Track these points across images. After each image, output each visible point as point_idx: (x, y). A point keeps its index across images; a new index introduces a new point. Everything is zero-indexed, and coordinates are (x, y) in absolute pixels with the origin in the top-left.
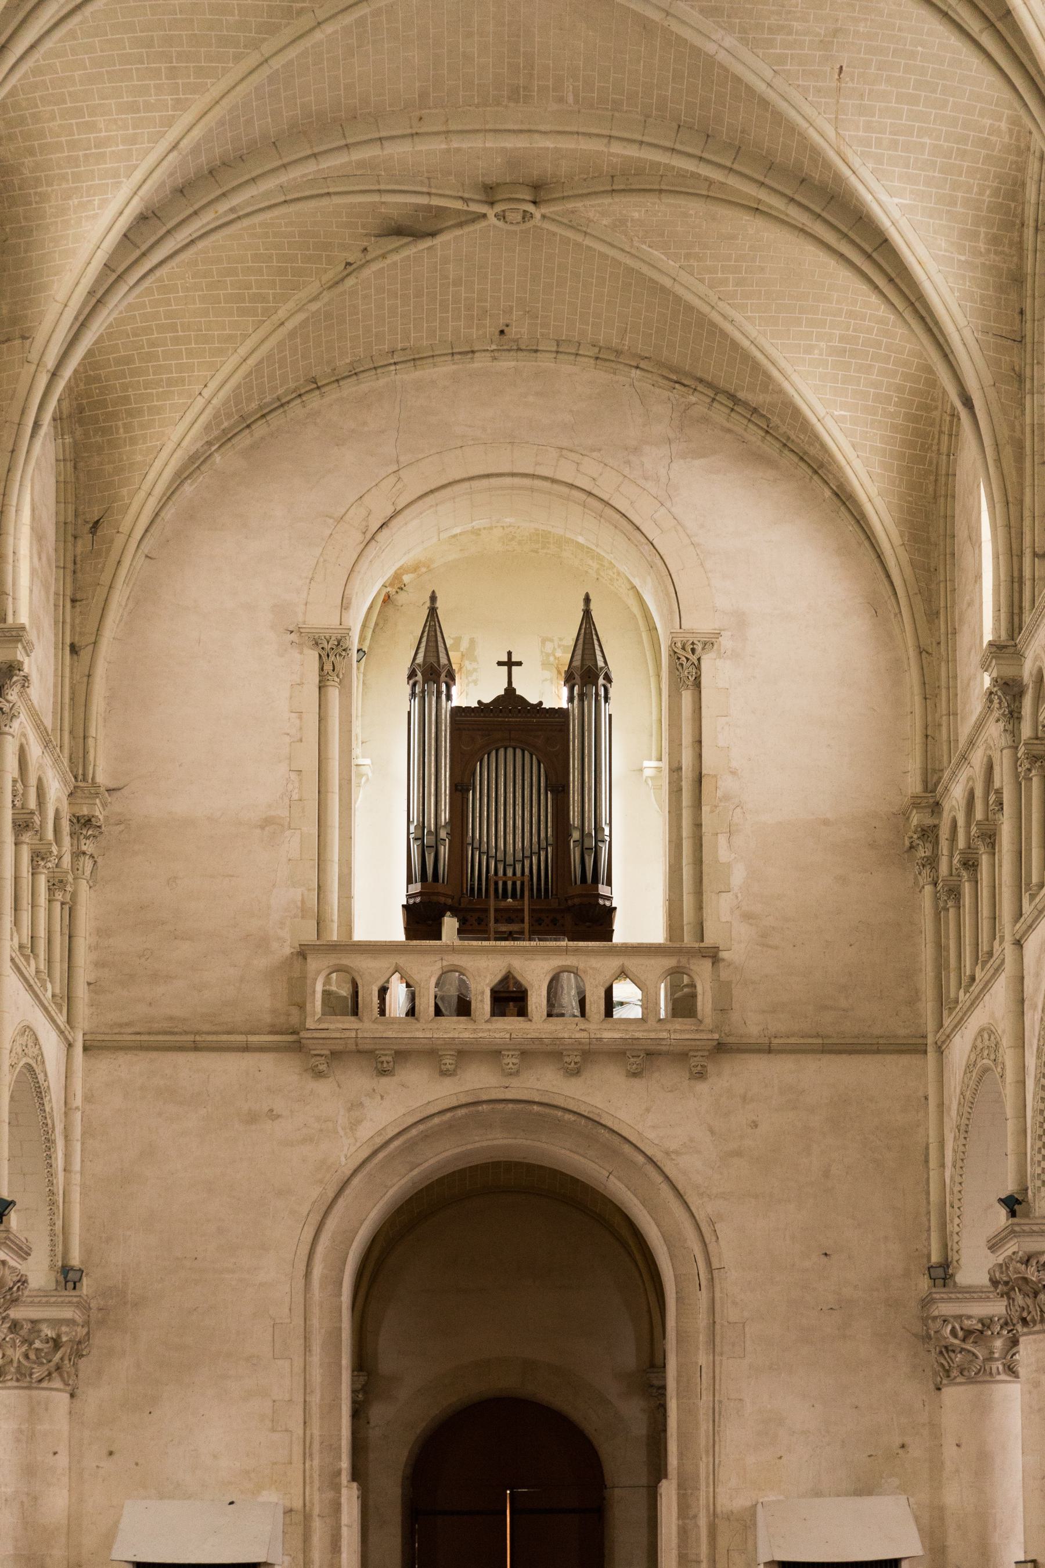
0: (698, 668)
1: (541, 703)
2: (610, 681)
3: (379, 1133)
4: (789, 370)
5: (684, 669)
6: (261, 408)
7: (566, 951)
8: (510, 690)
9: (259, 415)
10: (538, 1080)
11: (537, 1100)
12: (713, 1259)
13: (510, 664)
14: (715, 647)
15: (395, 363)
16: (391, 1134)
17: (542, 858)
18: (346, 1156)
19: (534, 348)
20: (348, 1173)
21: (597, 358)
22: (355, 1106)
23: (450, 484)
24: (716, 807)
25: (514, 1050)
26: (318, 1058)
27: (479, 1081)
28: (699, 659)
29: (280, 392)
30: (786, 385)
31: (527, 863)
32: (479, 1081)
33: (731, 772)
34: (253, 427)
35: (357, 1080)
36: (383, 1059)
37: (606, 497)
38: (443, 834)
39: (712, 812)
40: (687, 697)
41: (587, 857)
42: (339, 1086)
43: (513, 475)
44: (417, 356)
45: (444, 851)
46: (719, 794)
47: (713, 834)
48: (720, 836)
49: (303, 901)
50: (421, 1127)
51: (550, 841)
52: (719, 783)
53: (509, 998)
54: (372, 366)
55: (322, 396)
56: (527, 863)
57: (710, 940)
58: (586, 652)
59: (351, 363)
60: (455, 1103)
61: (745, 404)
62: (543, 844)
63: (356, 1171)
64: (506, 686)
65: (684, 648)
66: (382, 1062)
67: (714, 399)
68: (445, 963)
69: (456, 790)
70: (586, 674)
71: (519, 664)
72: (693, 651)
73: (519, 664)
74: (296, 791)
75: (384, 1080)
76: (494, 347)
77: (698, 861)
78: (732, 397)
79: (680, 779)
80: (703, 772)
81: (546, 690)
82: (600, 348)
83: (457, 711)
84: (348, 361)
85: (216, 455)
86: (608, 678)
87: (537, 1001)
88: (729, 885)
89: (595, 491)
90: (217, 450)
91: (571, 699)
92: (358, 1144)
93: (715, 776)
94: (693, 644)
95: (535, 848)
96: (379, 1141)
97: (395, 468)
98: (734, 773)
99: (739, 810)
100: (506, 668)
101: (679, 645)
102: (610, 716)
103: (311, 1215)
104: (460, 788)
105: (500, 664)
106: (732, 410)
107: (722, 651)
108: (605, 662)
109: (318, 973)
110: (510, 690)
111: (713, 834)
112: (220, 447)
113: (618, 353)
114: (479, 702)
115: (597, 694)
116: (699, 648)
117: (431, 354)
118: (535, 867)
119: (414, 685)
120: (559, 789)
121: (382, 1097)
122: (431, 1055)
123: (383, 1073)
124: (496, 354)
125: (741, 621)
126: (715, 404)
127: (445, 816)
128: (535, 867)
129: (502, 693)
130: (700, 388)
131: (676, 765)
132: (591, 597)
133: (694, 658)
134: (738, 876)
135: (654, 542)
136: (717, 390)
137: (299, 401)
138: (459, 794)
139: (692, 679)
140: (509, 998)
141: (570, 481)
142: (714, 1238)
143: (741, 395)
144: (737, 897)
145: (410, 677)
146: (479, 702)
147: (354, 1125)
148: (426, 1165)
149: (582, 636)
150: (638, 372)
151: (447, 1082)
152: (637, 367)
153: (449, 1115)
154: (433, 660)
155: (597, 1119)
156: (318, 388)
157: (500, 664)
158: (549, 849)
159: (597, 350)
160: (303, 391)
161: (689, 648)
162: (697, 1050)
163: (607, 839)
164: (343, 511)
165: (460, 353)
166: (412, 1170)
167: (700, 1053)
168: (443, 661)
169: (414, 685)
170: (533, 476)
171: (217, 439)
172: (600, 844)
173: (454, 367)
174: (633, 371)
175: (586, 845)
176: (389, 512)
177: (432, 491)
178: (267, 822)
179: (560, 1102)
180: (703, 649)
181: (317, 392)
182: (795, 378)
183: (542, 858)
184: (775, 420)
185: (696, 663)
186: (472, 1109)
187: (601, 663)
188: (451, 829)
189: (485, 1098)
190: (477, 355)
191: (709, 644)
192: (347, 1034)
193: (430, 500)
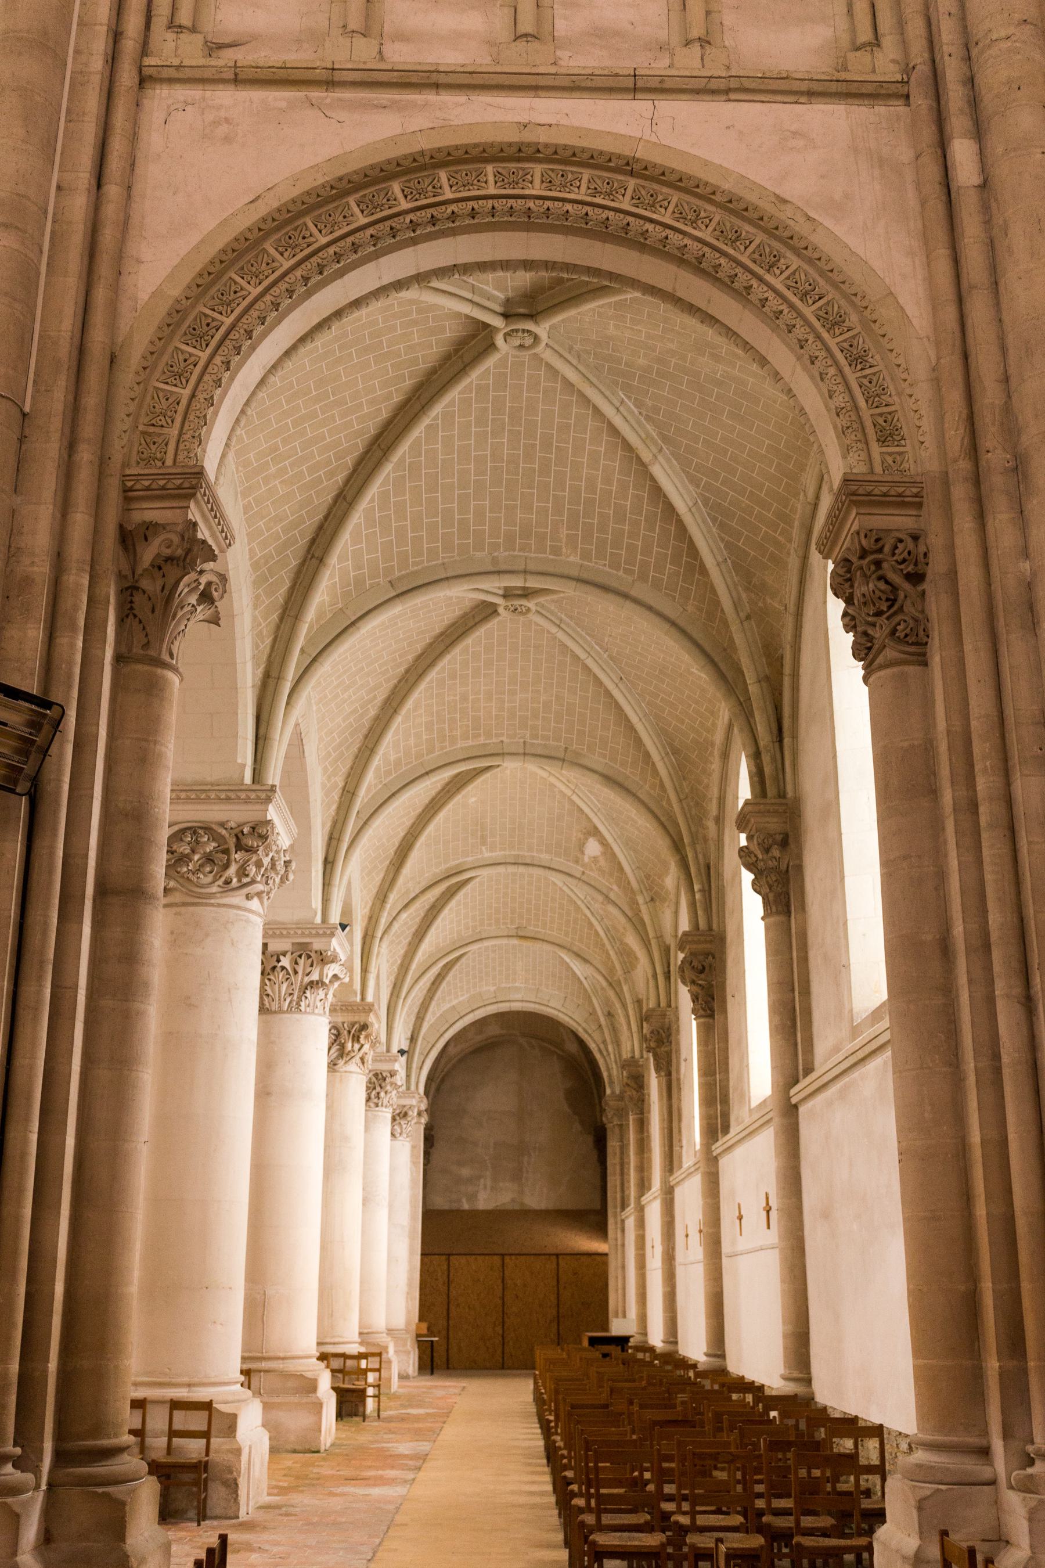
40: (644, 436)
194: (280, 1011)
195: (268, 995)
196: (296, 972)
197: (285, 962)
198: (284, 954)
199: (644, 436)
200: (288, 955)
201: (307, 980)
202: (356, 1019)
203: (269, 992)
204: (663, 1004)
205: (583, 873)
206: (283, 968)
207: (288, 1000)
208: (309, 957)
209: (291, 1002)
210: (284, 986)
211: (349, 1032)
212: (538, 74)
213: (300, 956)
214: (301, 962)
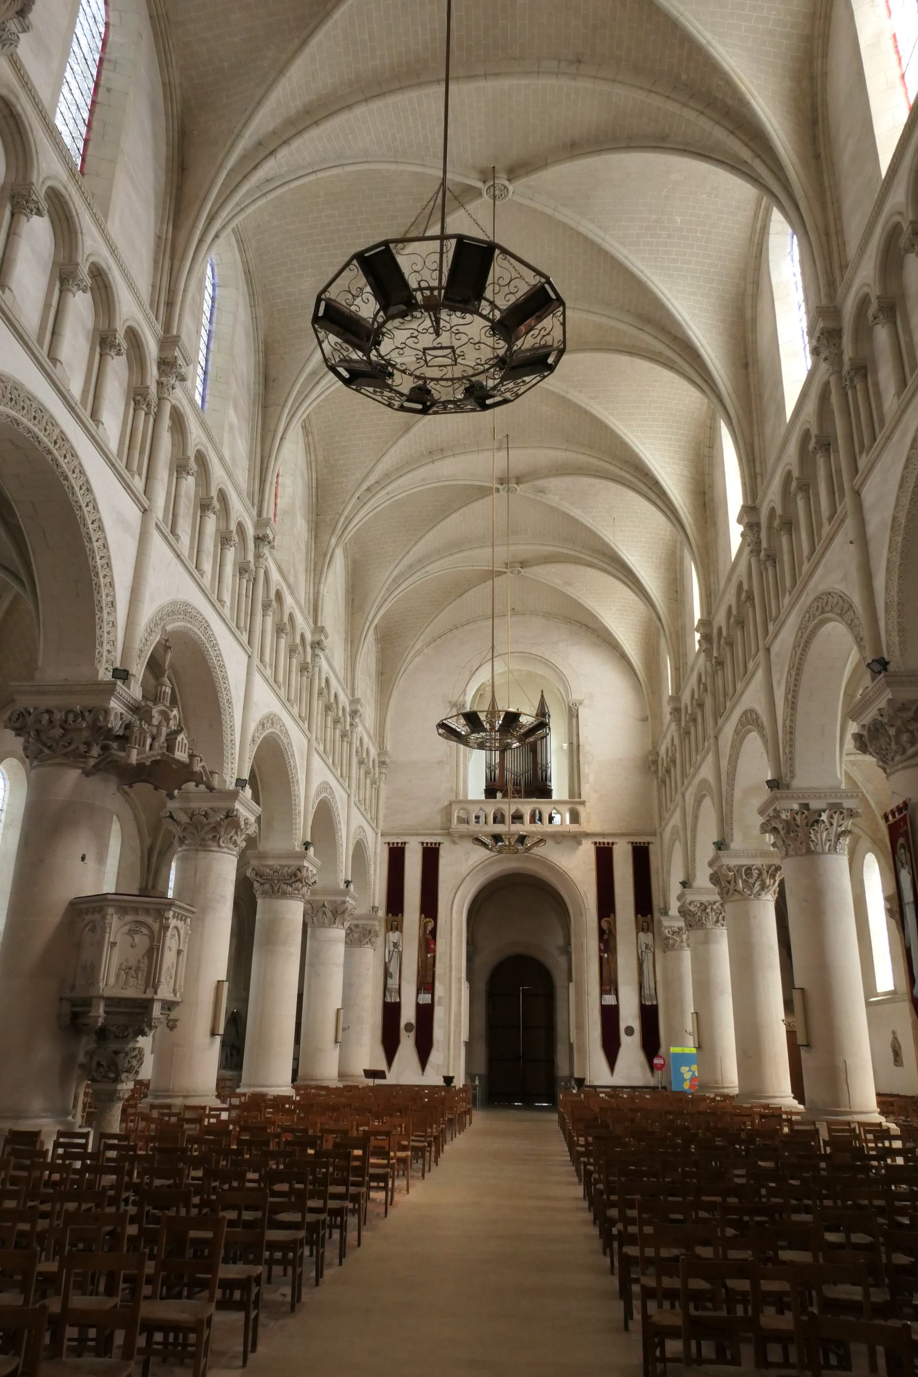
5: (573, 714)
40: (574, 720)
57: (583, 799)
87: (527, 818)
96: (475, 865)
134: (592, 778)
178: (440, 762)
194: (823, 852)
195: (812, 841)
196: (832, 824)
197: (824, 817)
198: (824, 811)
199: (574, 720)
200: (827, 812)
201: (840, 829)
202: (771, 863)
203: (814, 838)
204: (150, 886)
205: (113, 944)
206: (823, 821)
207: (828, 845)
208: (842, 813)
209: (830, 846)
210: (825, 834)
211: (768, 872)
212: (417, 835)
213: (835, 813)
214: (836, 817)
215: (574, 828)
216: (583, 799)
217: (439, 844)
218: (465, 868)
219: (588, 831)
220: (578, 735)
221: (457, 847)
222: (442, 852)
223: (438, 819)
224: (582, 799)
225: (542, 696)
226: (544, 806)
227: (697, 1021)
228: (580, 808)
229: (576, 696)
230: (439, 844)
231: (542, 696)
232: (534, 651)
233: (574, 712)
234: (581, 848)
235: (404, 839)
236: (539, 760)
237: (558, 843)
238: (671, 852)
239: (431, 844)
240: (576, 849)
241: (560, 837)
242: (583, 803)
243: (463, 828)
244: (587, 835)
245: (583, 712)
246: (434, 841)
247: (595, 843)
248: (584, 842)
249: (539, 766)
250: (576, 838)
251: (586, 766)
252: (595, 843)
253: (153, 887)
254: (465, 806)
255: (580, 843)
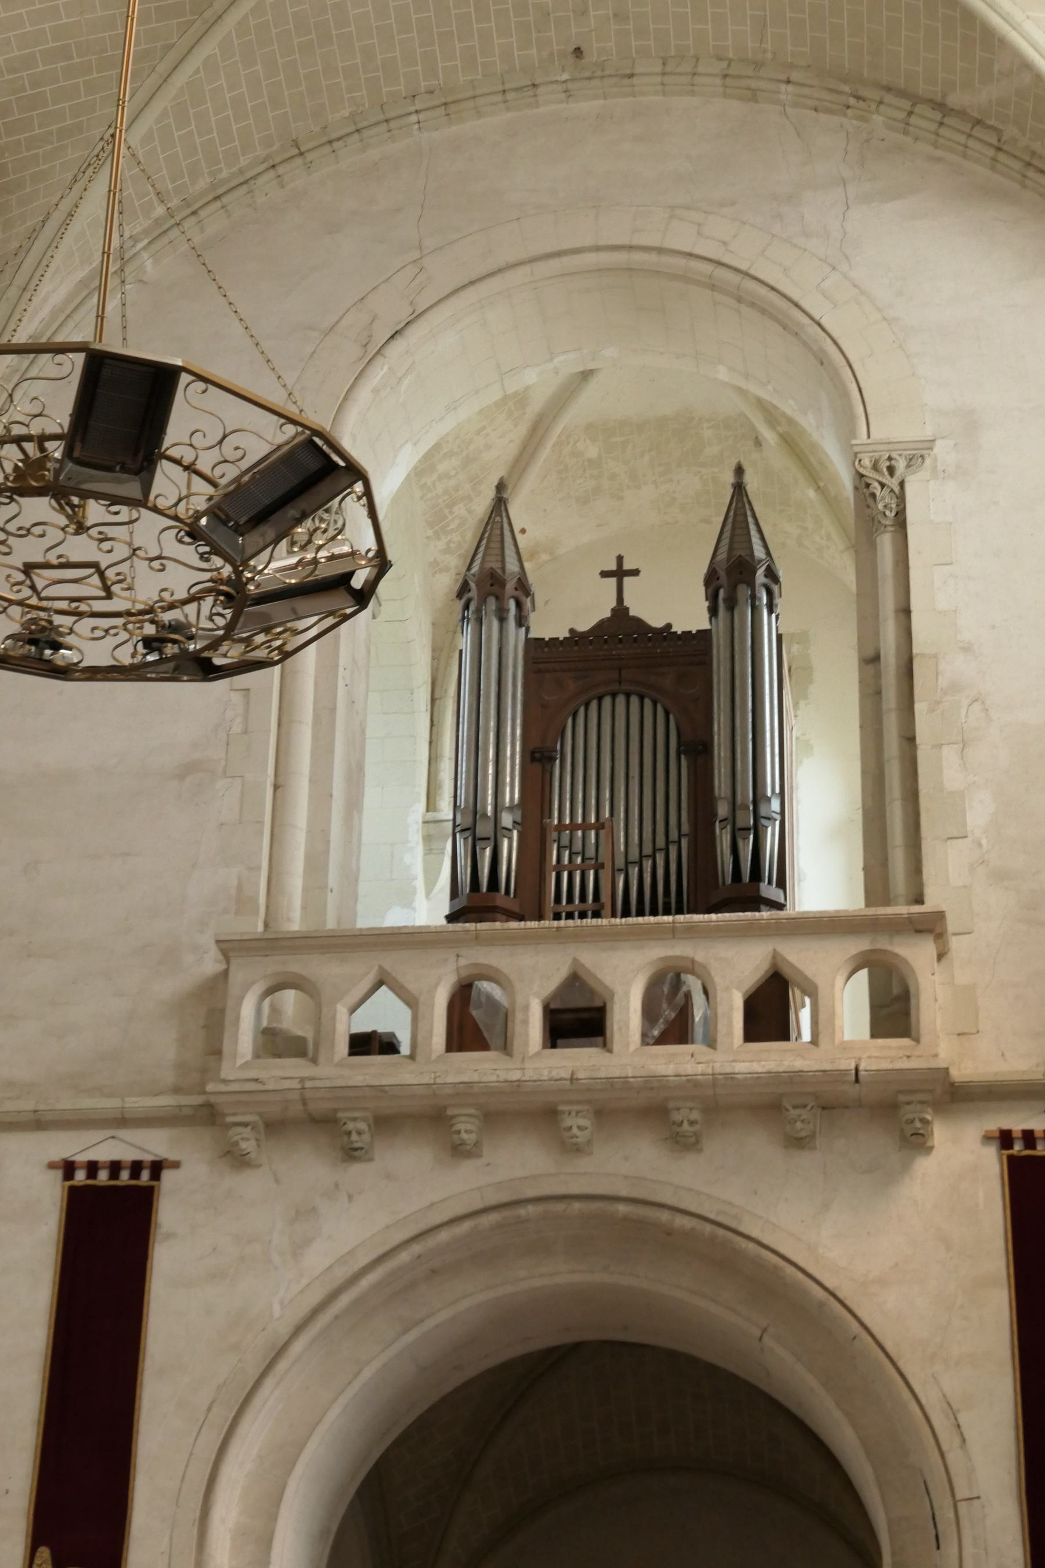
0: (901, 498)
1: (669, 626)
2: (776, 579)
3: (342, 1260)
4: (1019, 16)
5: (878, 513)
6: (213, 186)
7: (673, 932)
8: (620, 611)
9: (210, 197)
10: (626, 1158)
11: (624, 1193)
12: (958, 1482)
13: (620, 573)
14: (928, 461)
15: (417, 112)
16: (363, 1260)
17: (673, 856)
18: (281, 1303)
19: (628, 71)
20: (284, 1330)
21: (725, 76)
22: (304, 1213)
23: (500, 271)
24: (938, 703)
25: (579, 1102)
26: (240, 1129)
27: (519, 1164)
28: (902, 484)
29: (243, 161)
30: (1014, 37)
31: (648, 865)
32: (519, 1164)
33: (962, 648)
34: (203, 213)
35: (307, 1168)
36: (350, 1126)
37: (743, 267)
38: (507, 819)
39: (932, 710)
40: (886, 542)
41: (740, 843)
42: (277, 1181)
43: (597, 249)
44: (449, 99)
45: (509, 848)
46: (943, 682)
47: (934, 747)
48: (945, 750)
49: (240, 888)
50: (417, 1248)
51: (685, 828)
52: (942, 666)
53: (577, 1020)
54: (382, 117)
55: (308, 166)
56: (648, 865)
57: (933, 901)
58: (738, 532)
59: (352, 115)
60: (478, 1205)
61: (961, 113)
62: (674, 835)
63: (298, 1330)
64: (613, 603)
65: (875, 467)
66: (349, 1133)
67: (910, 113)
68: (463, 962)
69: (533, 759)
70: (737, 576)
71: (635, 573)
72: (891, 470)
73: (635, 573)
74: (239, 719)
75: (356, 1169)
76: (565, 76)
77: (912, 796)
78: (940, 106)
79: (878, 675)
80: (915, 651)
81: (673, 601)
82: (730, 61)
83: (535, 647)
84: (346, 113)
85: (145, 255)
86: (771, 574)
87: (627, 1016)
88: (965, 825)
89: (727, 259)
90: (144, 248)
91: (713, 611)
92: (304, 1282)
93: (935, 657)
94: (890, 459)
95: (661, 842)
96: (342, 1274)
97: (416, 255)
98: (967, 649)
99: (977, 706)
100: (613, 581)
101: (867, 462)
102: (779, 637)
103: (214, 1410)
104: (539, 758)
105: (605, 574)
106: (941, 124)
107: (940, 468)
108: (768, 553)
109: (247, 987)
110: (620, 611)
111: (934, 747)
112: (150, 243)
113: (758, 65)
114: (572, 631)
115: (754, 597)
116: (901, 465)
117: (470, 94)
118: (660, 872)
119: (467, 607)
120: (697, 749)
121: (350, 1198)
122: (429, 1119)
123: (351, 1154)
124: (570, 85)
125: (970, 424)
126: (913, 120)
127: (512, 793)
128: (660, 872)
129: (608, 614)
130: (889, 98)
131: (870, 653)
132: (744, 467)
133: (893, 483)
134: (979, 814)
135: (823, 322)
136: (916, 100)
137: (272, 174)
138: (537, 767)
139: (891, 515)
140: (577, 1020)
141: (687, 249)
142: (957, 1441)
143: (954, 100)
144: (980, 845)
145: (460, 595)
146: (572, 631)
147: (298, 1248)
148: (430, 1324)
149: (730, 520)
150: (790, 88)
151: (467, 1167)
152: (788, 82)
153: (467, 1225)
154: (496, 566)
155: (733, 1224)
156: (301, 154)
157: (605, 574)
158: (684, 842)
159: (725, 64)
160: (278, 160)
161: (884, 465)
162: (913, 1092)
163: (778, 817)
164: (335, 318)
165: (517, 90)
166: (406, 1331)
167: (919, 1097)
168: (512, 566)
169: (467, 607)
170: (630, 248)
171: (146, 232)
172: (764, 822)
173: (510, 115)
174: (783, 87)
175: (740, 824)
176: (404, 315)
177: (472, 283)
178: (187, 769)
179: (666, 1196)
180: (908, 466)
181: (299, 161)
182: (1029, 27)
183: (673, 856)
184: (1010, 131)
185: (897, 489)
186: (507, 1213)
187: (759, 552)
188: (523, 817)
189: (531, 1193)
190: (541, 90)
191: (915, 460)
192: (287, 1084)
193: (470, 296)
199: (886, 542)
215: (889, 1055)
216: (933, 901)
217: (157, 1168)
218: (282, 1292)
219: (961, 1073)
220: (905, 611)
221: (251, 1184)
222: (168, 1213)
223: (163, 1049)
224: (930, 905)
225: (739, 488)
226: (731, 963)
227: (180, 62)
228: (917, 955)
229: (890, 428)
230: (157, 1168)
231: (739, 488)
232: (682, 238)
233: (885, 500)
234: (925, 1166)
235: (152, 1144)
236: (721, 785)
237: (797, 1143)
238: (241, 999)
239: (115, 1167)
240: (886, 1178)
241: (812, 1114)
242: (932, 927)
243: (285, 1073)
244: (956, 1096)
245: (926, 502)
246: (126, 1154)
247: (1005, 1139)
248: (941, 1133)
249: (723, 810)
250: (895, 1112)
251: (950, 755)
252: (1005, 1139)
253: (931, 1091)
254: (295, 965)
255: (916, 1141)
